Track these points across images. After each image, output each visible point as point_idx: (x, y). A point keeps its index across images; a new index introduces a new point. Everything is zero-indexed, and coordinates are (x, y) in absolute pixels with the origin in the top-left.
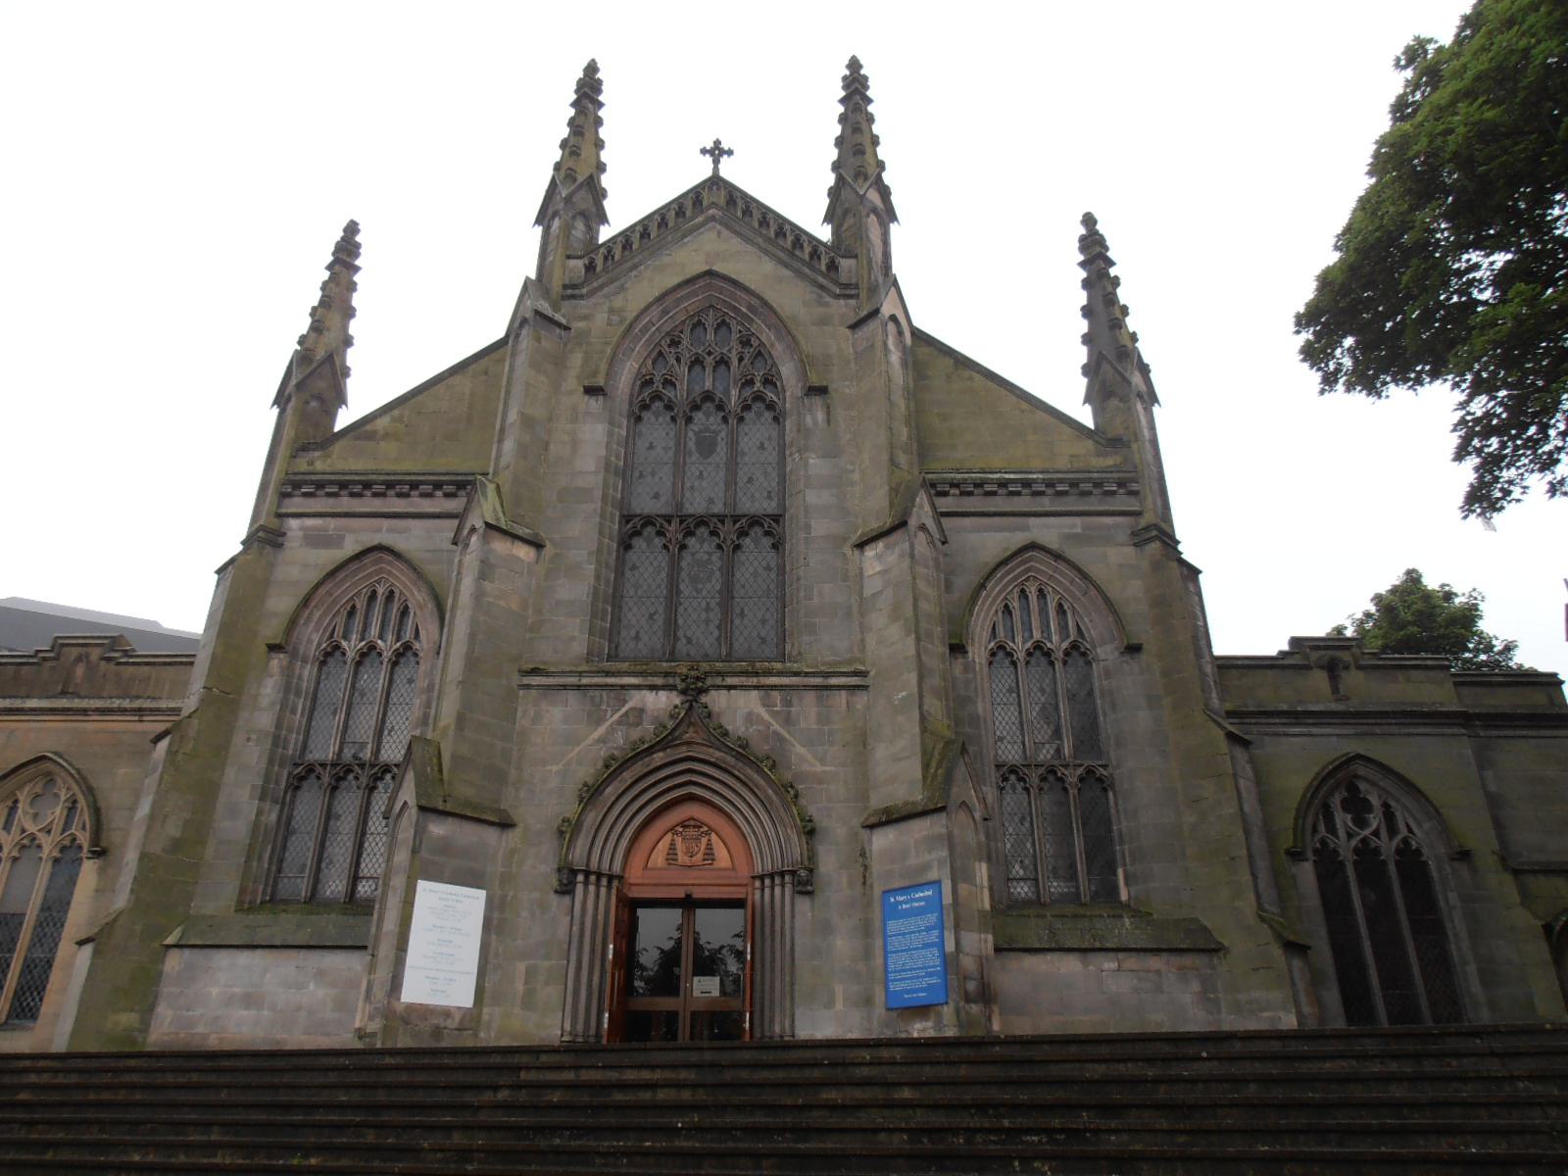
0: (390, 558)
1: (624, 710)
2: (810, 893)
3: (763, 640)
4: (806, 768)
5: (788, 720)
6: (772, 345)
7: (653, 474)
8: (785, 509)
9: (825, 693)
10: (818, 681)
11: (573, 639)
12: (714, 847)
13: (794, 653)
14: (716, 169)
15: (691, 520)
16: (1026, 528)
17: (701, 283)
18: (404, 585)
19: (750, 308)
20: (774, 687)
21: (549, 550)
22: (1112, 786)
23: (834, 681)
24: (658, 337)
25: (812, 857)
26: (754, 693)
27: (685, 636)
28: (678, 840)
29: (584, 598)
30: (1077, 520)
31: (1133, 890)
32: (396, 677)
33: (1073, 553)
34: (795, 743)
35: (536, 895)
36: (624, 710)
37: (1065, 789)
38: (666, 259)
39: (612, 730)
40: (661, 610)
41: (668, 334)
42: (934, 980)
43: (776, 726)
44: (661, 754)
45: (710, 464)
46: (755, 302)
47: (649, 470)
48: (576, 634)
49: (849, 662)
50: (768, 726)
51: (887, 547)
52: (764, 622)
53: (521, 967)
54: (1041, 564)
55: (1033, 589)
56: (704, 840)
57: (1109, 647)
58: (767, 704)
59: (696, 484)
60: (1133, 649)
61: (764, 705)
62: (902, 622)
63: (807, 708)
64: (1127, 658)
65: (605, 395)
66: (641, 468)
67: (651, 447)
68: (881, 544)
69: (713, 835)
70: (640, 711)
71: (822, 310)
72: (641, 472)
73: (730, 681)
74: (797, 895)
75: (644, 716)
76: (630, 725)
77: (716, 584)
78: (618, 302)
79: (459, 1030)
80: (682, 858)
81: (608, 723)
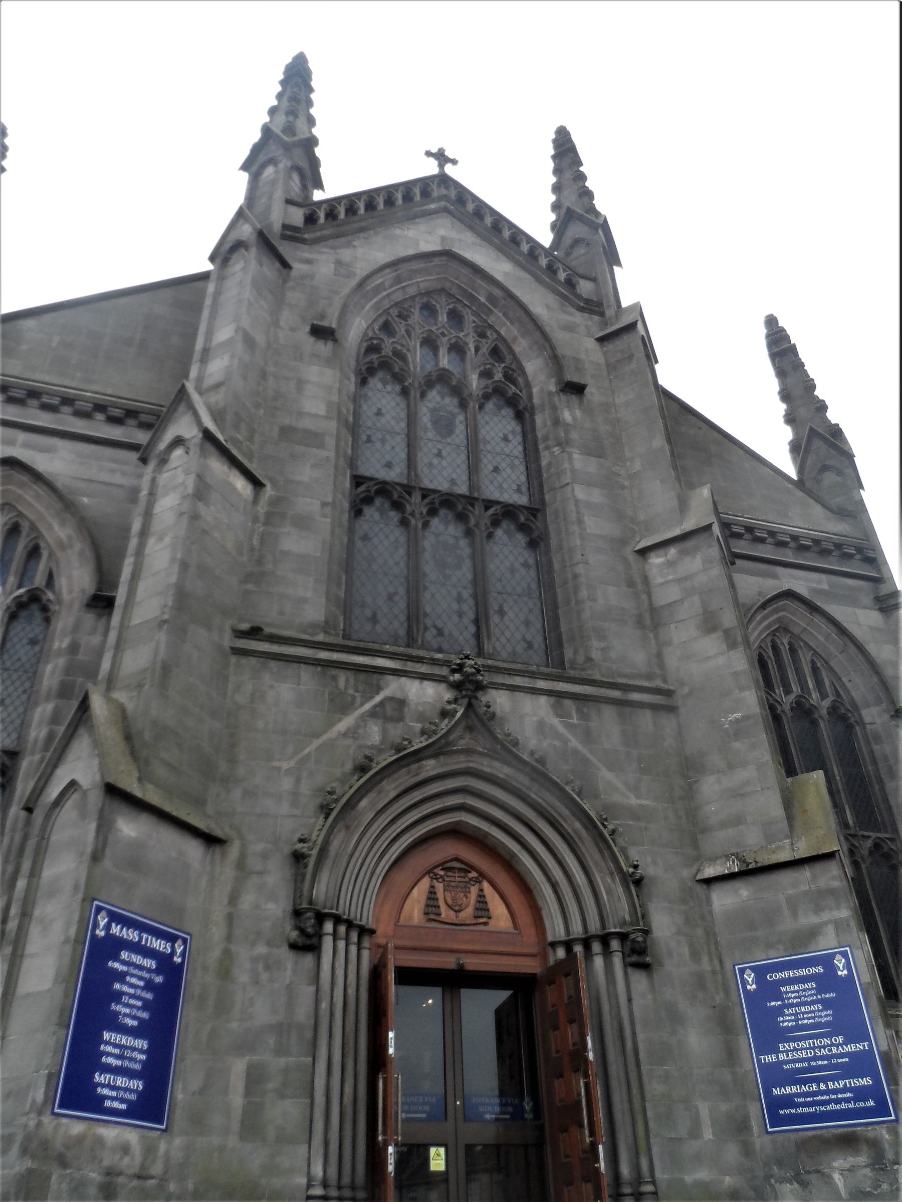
1: (378, 699)
3: (530, 645)
4: (616, 798)
5: (588, 737)
8: (543, 501)
10: (616, 694)
11: (304, 600)
12: (490, 906)
13: (581, 659)
15: (437, 495)
16: (775, 576)
17: (437, 261)
19: (491, 298)
21: (269, 491)
24: (386, 304)
25: (641, 916)
26: (543, 700)
27: (435, 627)
28: (440, 887)
29: (318, 554)
32: (12, 633)
33: (833, 609)
34: (599, 765)
35: (262, 949)
36: (378, 699)
38: (398, 232)
40: (402, 591)
41: (397, 304)
43: (575, 742)
44: (431, 762)
45: (449, 444)
46: (497, 292)
47: (379, 435)
48: (309, 594)
49: (649, 677)
50: (565, 741)
52: (527, 623)
53: (239, 1067)
54: (799, 618)
55: (785, 642)
56: (474, 890)
57: (874, 710)
61: (558, 715)
62: (721, 633)
65: (335, 340)
66: (369, 432)
67: (379, 413)
68: (672, 551)
69: (486, 885)
72: (369, 437)
73: (518, 681)
74: (630, 970)
75: (406, 710)
76: (387, 719)
77: (465, 573)
78: (346, 254)
79: (139, 1177)
80: (445, 913)
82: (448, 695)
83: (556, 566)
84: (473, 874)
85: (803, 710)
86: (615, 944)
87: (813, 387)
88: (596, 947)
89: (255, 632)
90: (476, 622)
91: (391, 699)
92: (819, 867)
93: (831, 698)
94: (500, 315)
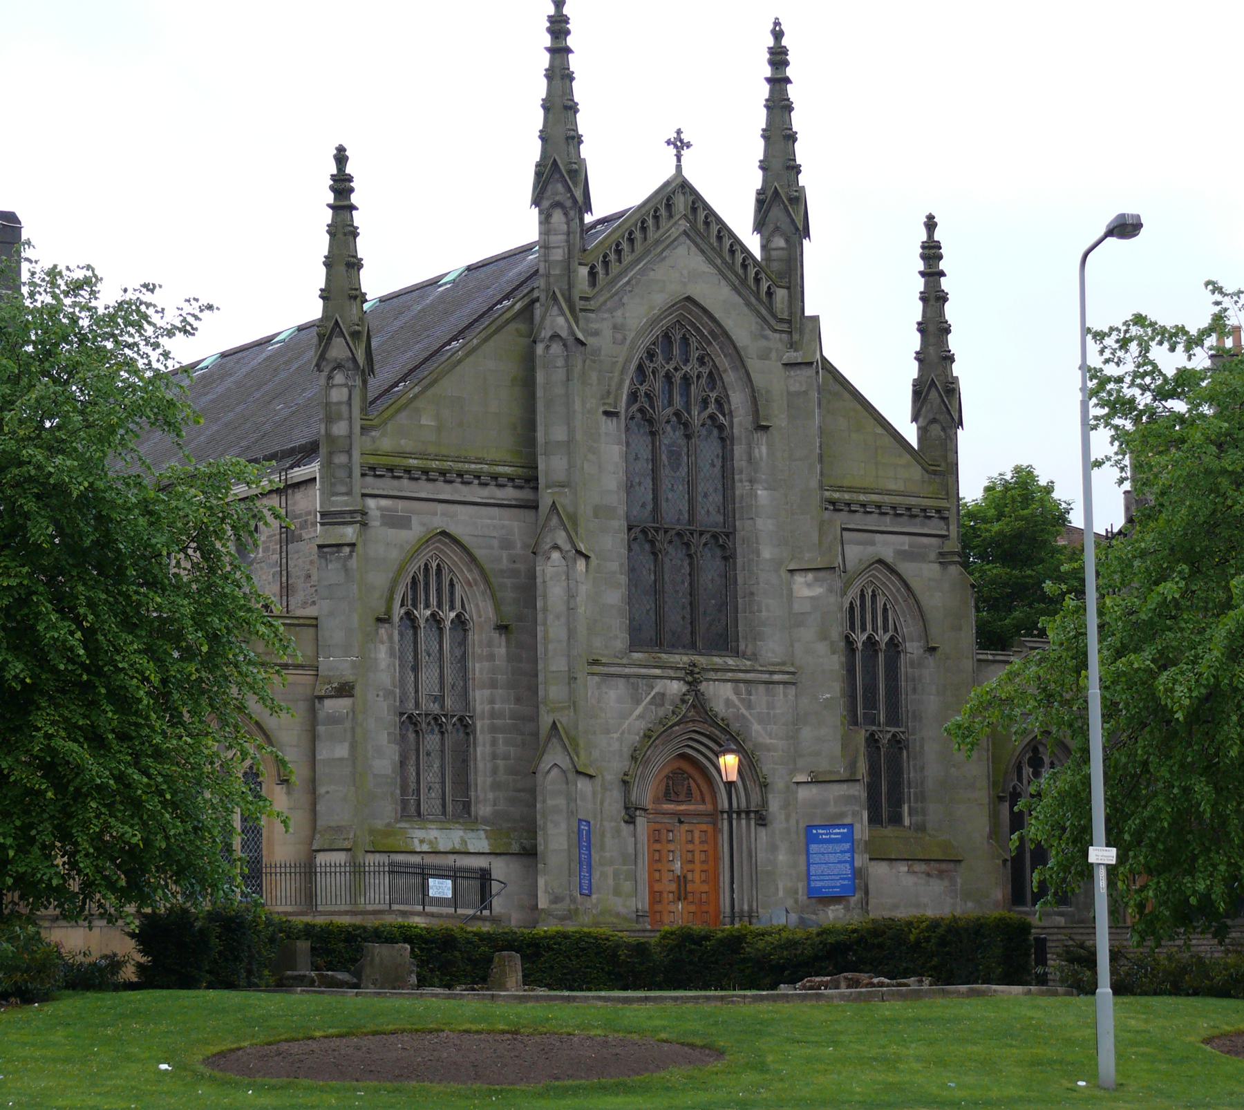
0: (447, 541)
1: (653, 694)
2: (764, 825)
4: (760, 740)
5: (749, 706)
6: (725, 371)
7: (640, 484)
9: (771, 686)
10: (765, 677)
13: (749, 652)
14: (679, 168)
16: (873, 543)
18: (455, 564)
19: (712, 332)
20: (746, 682)
22: (907, 748)
23: (776, 677)
25: (765, 803)
30: (906, 539)
31: (914, 819)
35: (613, 824)
37: (878, 748)
39: (646, 709)
42: (846, 882)
43: (743, 711)
47: (637, 480)
49: (784, 664)
51: (816, 580)
57: (916, 644)
58: (737, 693)
59: (670, 496)
60: (932, 650)
63: (760, 696)
64: (927, 655)
68: (810, 576)
70: (662, 695)
71: (764, 343)
81: (644, 703)
82: (684, 688)
83: (740, 581)
84: (685, 775)
85: (871, 643)
86: (752, 815)
87: (947, 330)
88: (743, 816)
89: (596, 662)
90: (691, 623)
91: (658, 693)
92: (851, 784)
93: (891, 633)
94: (717, 347)
